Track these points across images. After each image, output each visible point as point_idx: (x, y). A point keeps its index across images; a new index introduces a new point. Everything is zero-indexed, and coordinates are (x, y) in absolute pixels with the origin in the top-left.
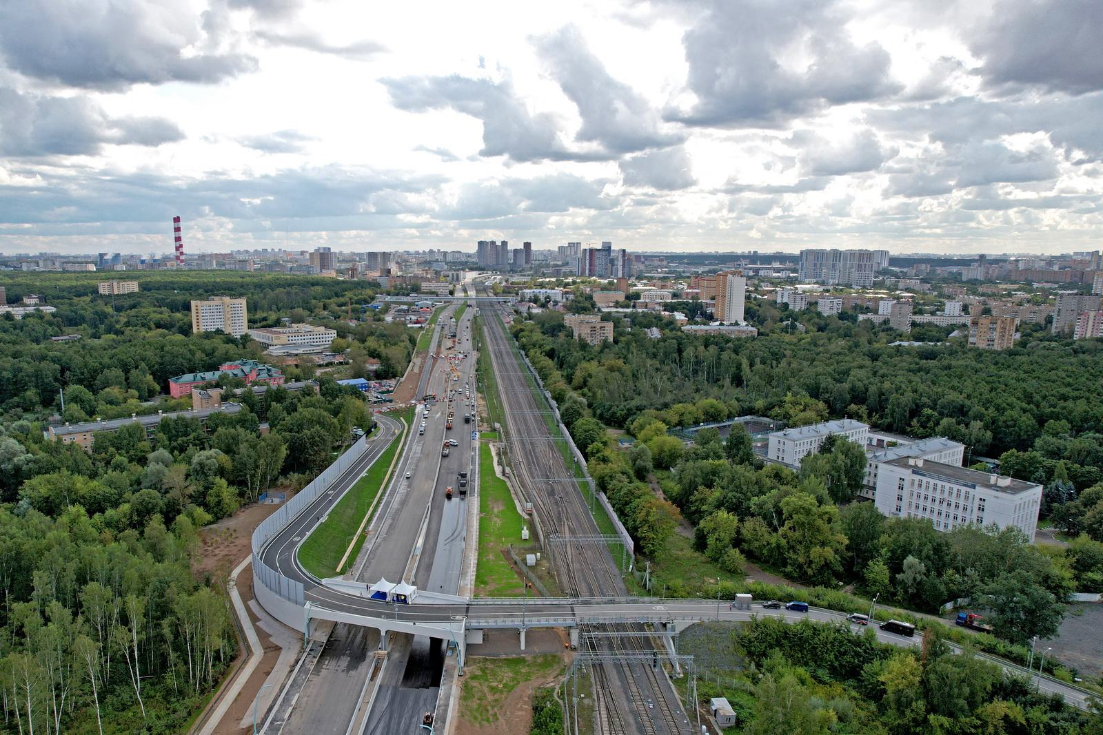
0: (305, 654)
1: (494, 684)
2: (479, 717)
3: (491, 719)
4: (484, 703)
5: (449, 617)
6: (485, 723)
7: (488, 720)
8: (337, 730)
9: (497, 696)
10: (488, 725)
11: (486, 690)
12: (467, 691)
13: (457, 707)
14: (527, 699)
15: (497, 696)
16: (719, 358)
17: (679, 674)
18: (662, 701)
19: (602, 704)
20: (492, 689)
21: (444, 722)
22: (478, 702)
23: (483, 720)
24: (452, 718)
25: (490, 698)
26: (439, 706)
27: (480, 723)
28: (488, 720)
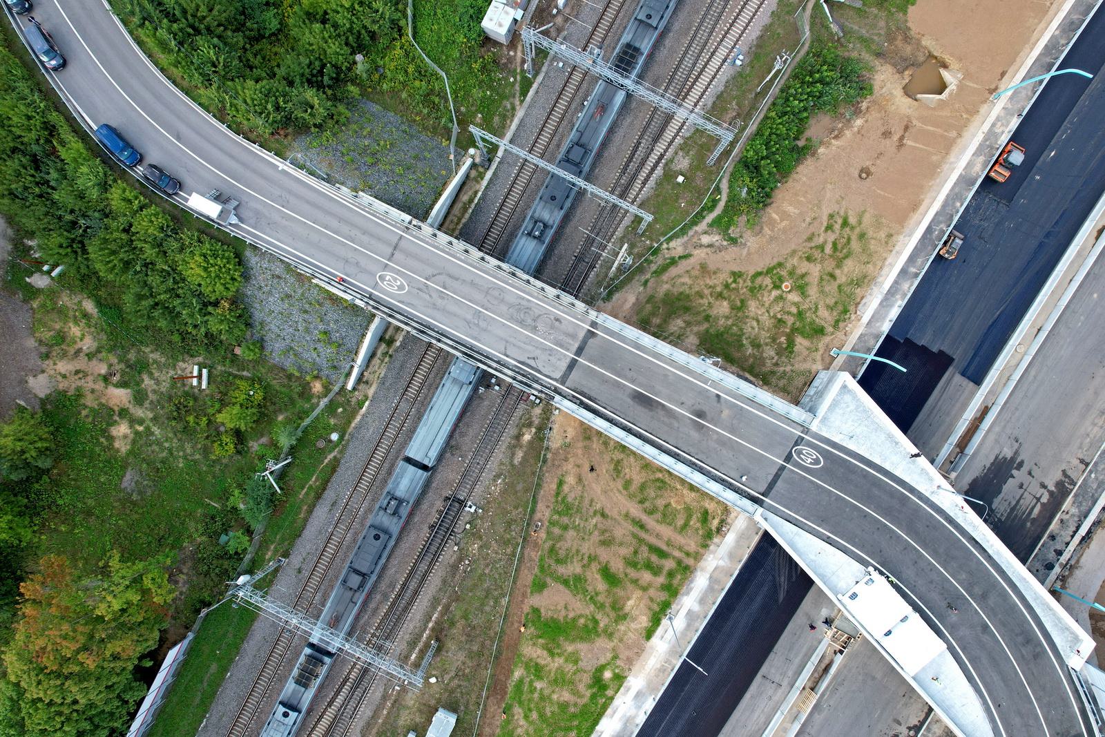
0: (1064, 558)
1: (794, 297)
2: (854, 237)
3: (840, 221)
4: (830, 265)
5: (823, 474)
6: (852, 220)
7: (845, 223)
8: (1092, 294)
9: (804, 267)
10: (850, 213)
11: (813, 291)
12: (845, 308)
13: (884, 272)
14: (767, 230)
15: (804, 267)
16: (98, 351)
17: (473, 157)
18: (562, 104)
19: (660, 148)
20: (801, 289)
21: (929, 230)
22: (837, 272)
23: (853, 228)
24: (910, 235)
25: (815, 270)
26: (916, 275)
27: (860, 223)
28: (845, 223)
